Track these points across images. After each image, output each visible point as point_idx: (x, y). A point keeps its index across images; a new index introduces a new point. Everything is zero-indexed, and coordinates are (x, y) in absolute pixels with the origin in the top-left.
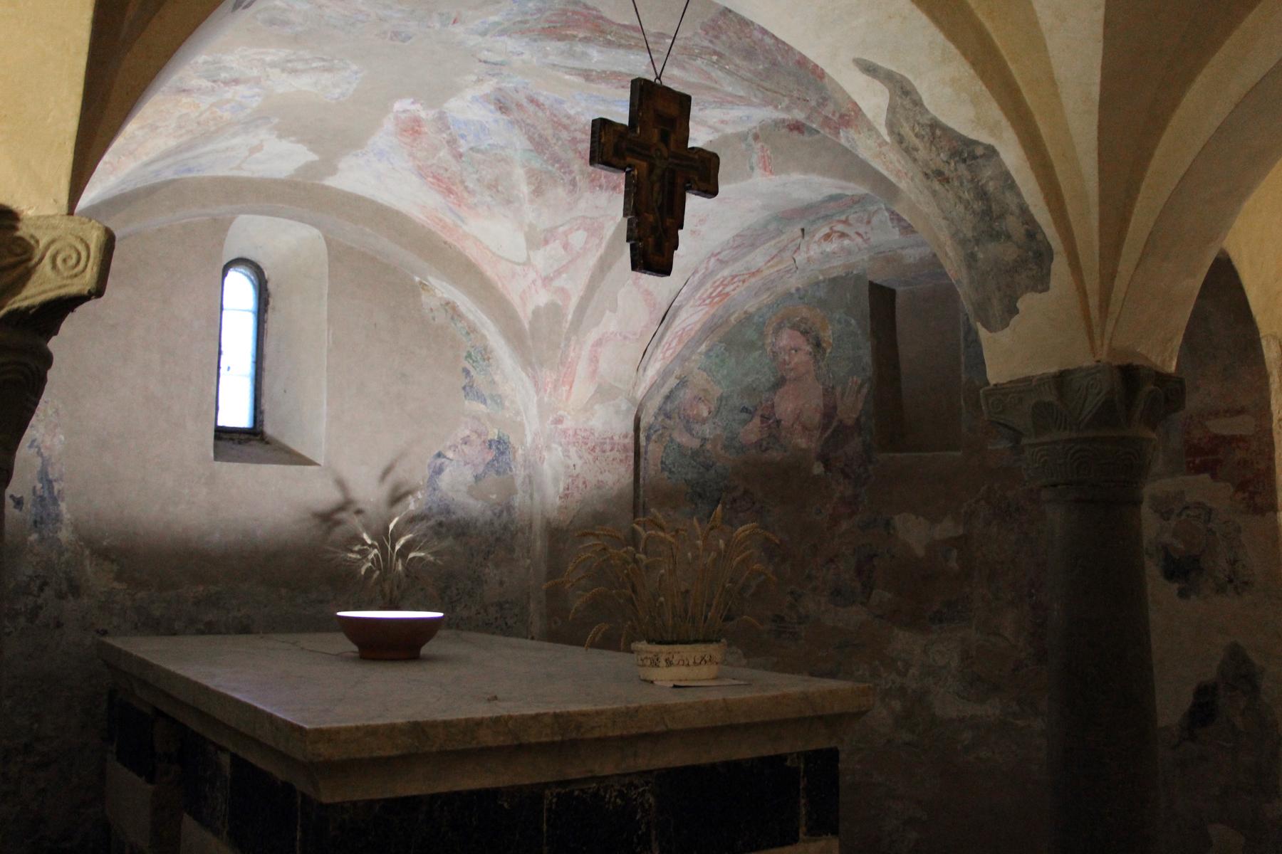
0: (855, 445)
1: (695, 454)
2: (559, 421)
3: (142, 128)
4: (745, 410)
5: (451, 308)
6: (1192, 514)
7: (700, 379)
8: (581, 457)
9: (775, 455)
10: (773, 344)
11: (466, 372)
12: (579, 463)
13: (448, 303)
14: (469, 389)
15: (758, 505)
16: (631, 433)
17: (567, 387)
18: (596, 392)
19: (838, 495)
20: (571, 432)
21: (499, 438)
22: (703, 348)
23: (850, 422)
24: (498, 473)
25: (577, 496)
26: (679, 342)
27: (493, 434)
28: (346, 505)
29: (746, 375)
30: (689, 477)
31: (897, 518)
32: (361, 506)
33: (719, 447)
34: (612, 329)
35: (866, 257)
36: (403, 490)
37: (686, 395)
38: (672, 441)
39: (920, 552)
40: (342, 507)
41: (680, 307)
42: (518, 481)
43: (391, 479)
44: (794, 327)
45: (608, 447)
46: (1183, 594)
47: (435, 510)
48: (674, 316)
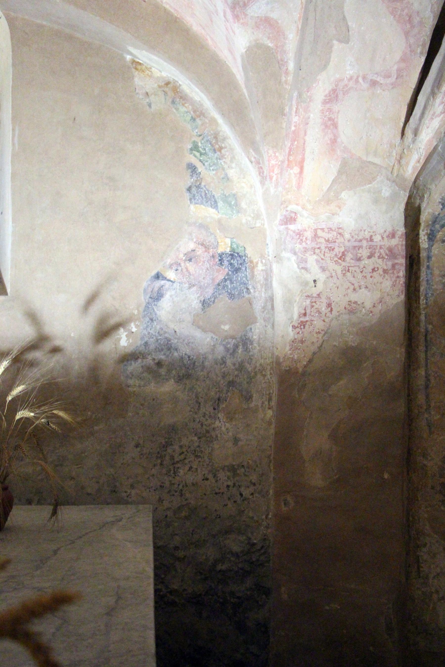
2: (290, 219)
5: (171, 89)
8: (323, 269)
11: (192, 168)
12: (322, 277)
13: (168, 84)
14: (197, 191)
16: (401, 230)
17: (296, 170)
18: (340, 173)
20: (309, 234)
21: (233, 250)
24: (231, 296)
25: (319, 324)
27: (225, 246)
28: (39, 342)
32: (58, 343)
34: (350, 71)
36: (112, 322)
40: (34, 346)
42: (258, 306)
43: (96, 310)
45: (365, 253)
47: (152, 347)
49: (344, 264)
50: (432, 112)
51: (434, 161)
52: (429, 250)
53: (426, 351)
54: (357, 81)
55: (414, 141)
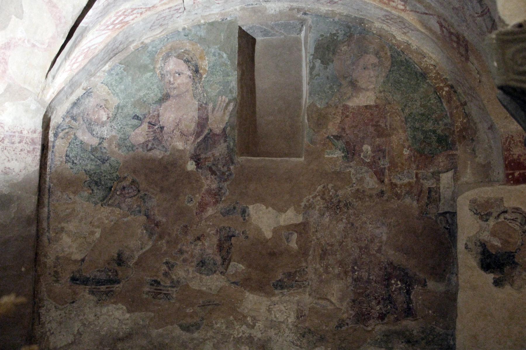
0: (220, 150)
1: (94, 150)
4: (136, 117)
6: (509, 217)
7: (102, 91)
9: (158, 153)
10: (162, 68)
15: (142, 193)
16: (40, 129)
19: (206, 187)
22: (107, 67)
23: (217, 131)
29: (139, 90)
30: (88, 168)
31: (251, 207)
33: (113, 146)
35: (238, 8)
37: (90, 103)
38: (76, 138)
39: (268, 234)
41: (86, 29)
44: (179, 57)
45: (17, 140)
46: (497, 283)
48: (82, 35)
49: (3, 145)
50: (63, 69)
51: (61, 95)
52: (54, 142)
53: (49, 198)
54: (24, 42)
55: (52, 82)
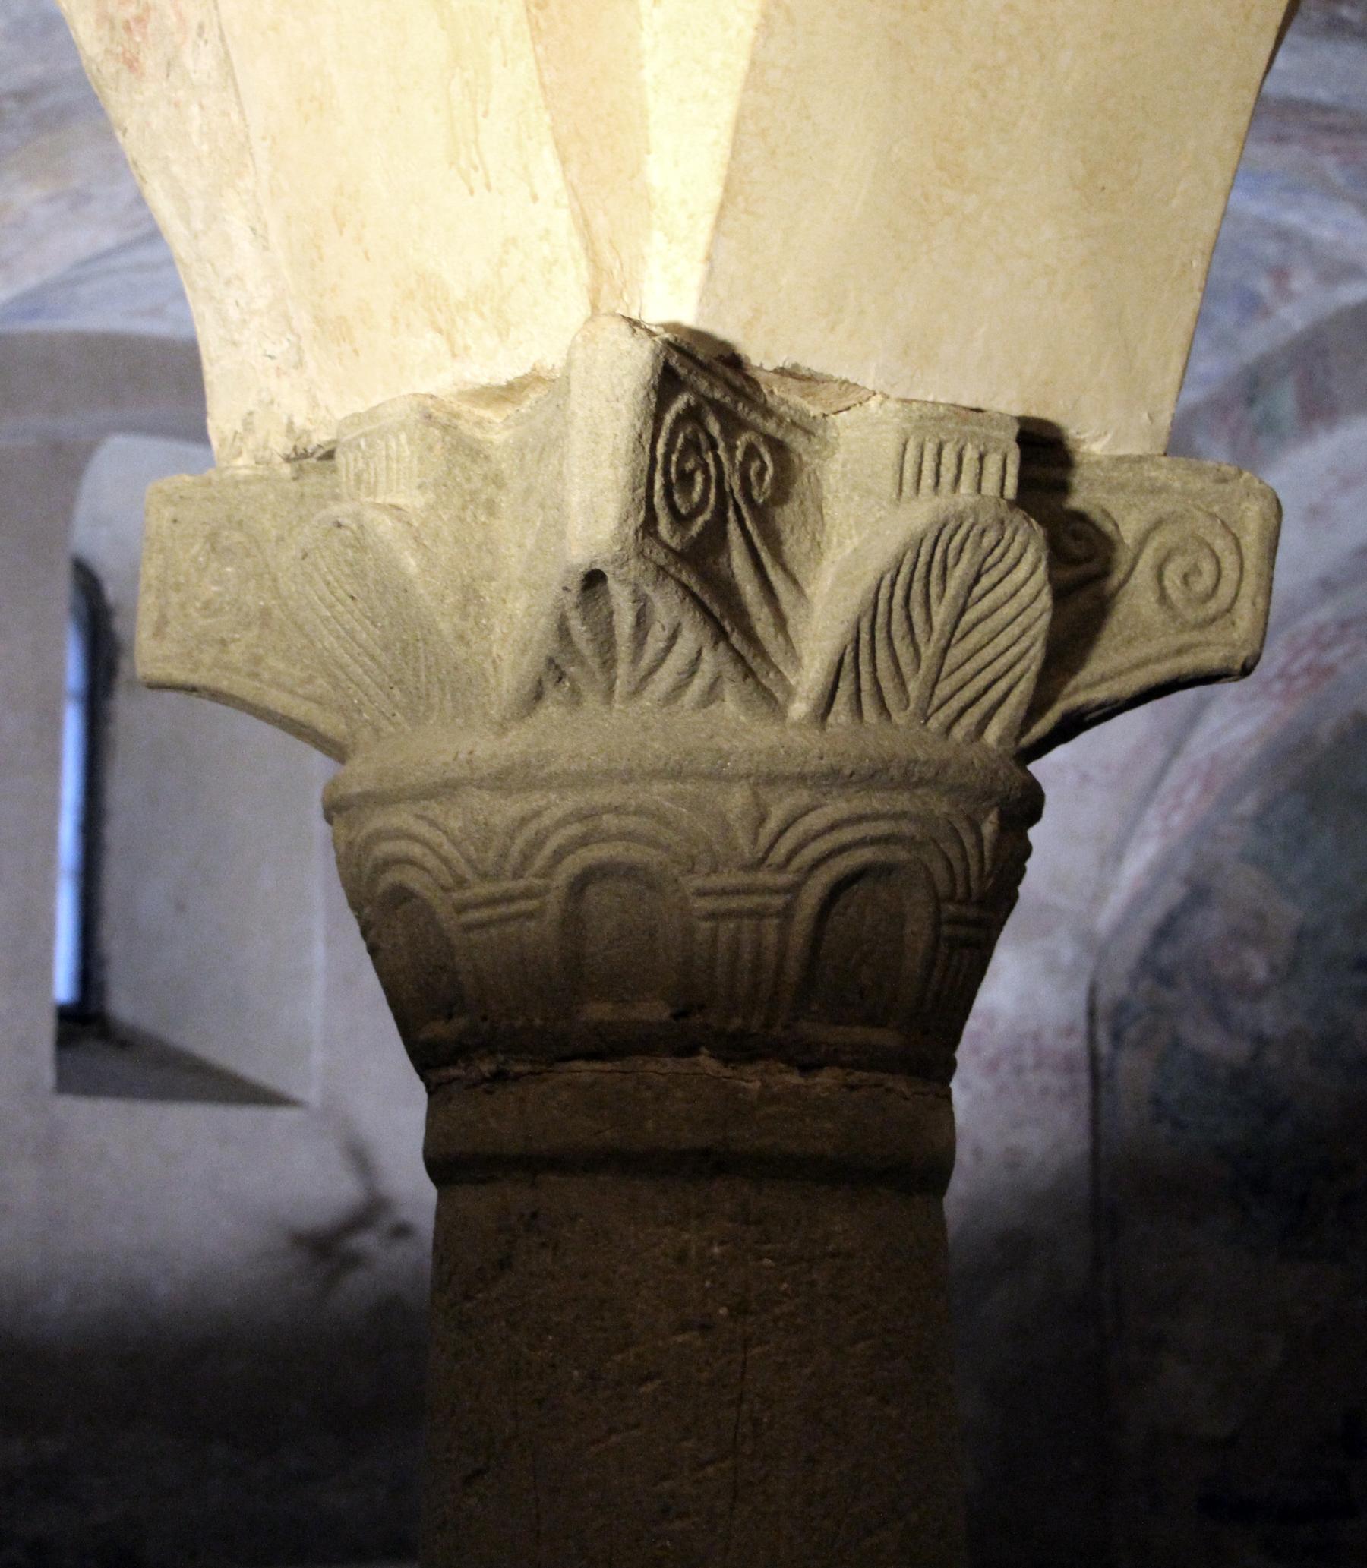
3: (50, 199)
16: (1082, 1024)
26: (1207, 788)
37: (1211, 924)
38: (1177, 1043)
45: (1029, 1060)
